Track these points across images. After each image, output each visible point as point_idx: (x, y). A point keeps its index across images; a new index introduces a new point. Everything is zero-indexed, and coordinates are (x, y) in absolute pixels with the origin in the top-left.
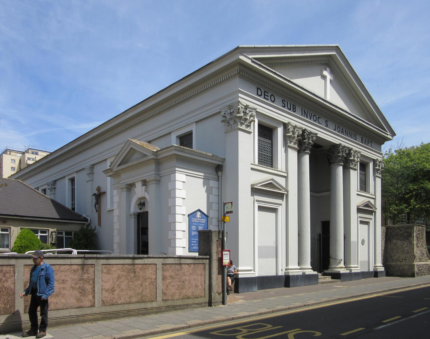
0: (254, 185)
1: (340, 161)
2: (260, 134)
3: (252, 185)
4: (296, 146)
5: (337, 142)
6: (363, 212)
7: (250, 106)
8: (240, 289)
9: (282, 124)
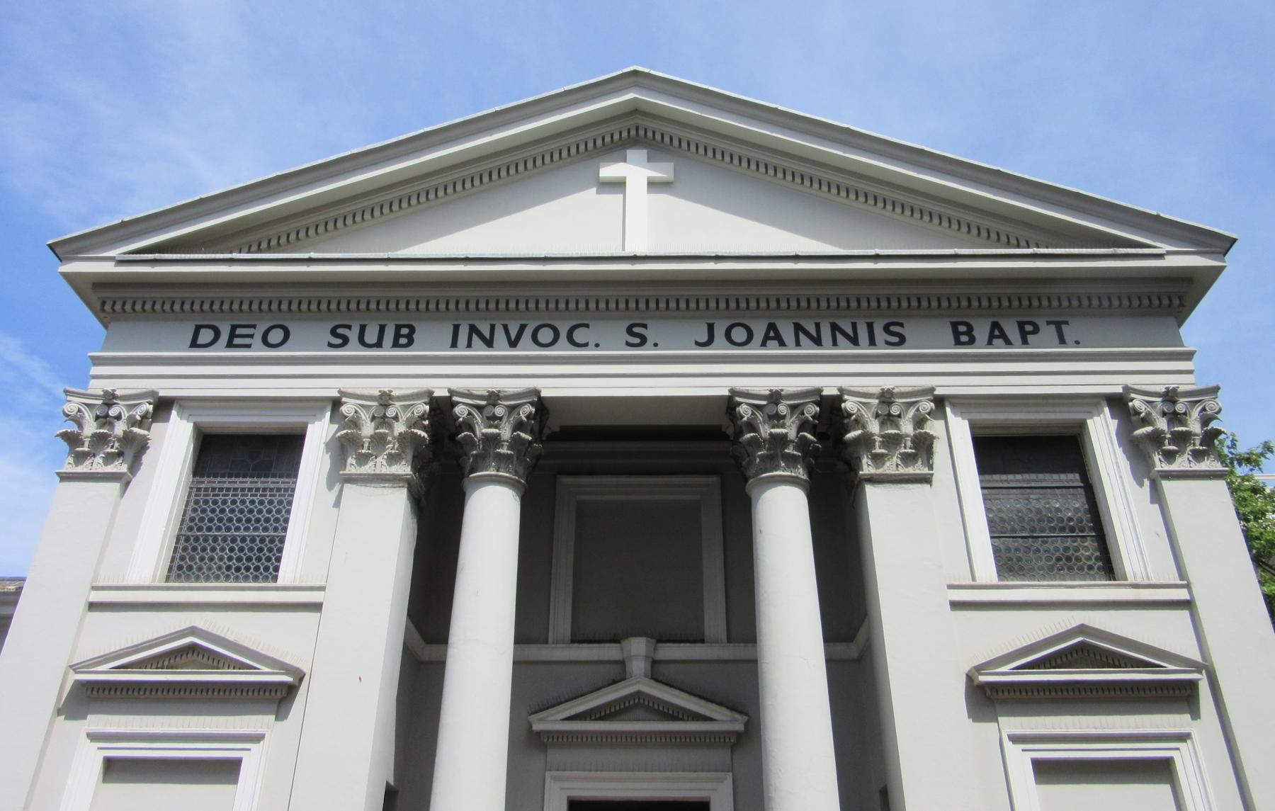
0: (979, 669)
1: (771, 461)
2: (984, 466)
3: (970, 678)
5: (719, 388)
6: (1038, 702)
7: (1182, 389)
9: (1104, 403)
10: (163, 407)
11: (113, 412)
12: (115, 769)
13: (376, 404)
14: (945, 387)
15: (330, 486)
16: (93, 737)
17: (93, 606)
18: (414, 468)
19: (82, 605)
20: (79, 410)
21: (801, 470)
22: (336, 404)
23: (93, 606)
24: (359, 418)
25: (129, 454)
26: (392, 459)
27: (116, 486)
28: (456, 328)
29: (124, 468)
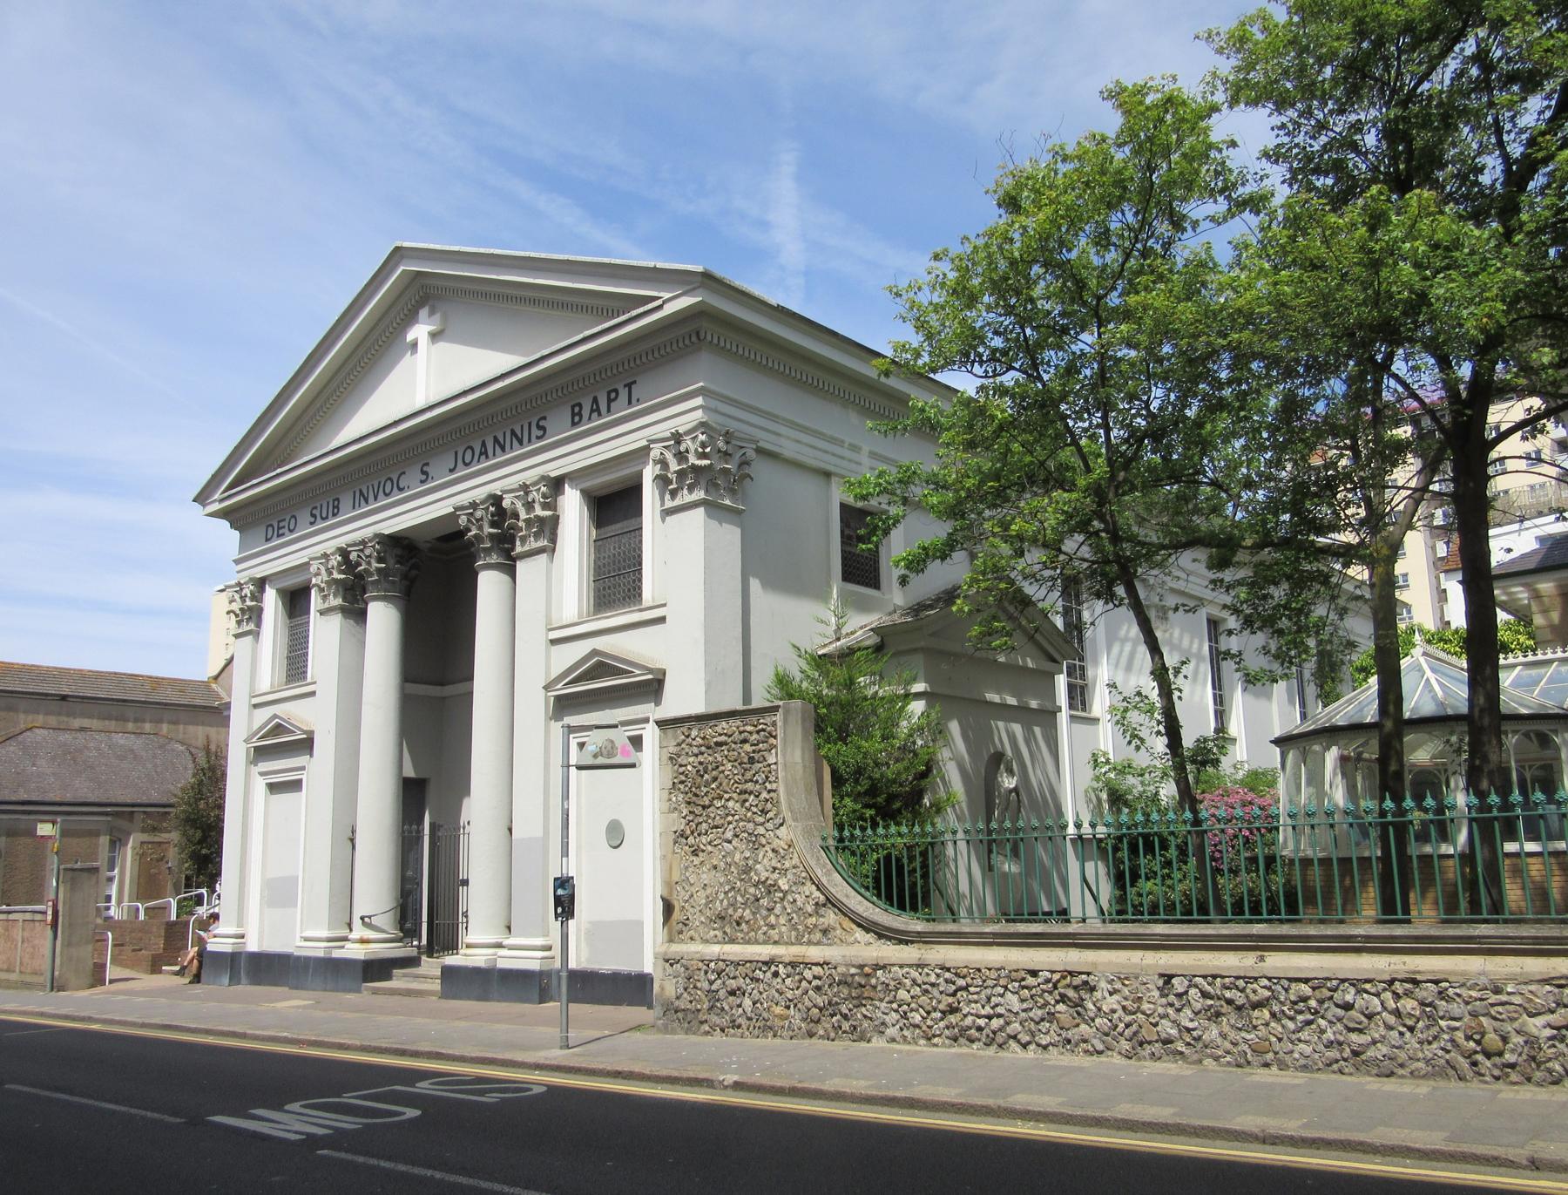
4: (338, 601)
12: (274, 788)
14: (554, 469)
16: (262, 774)
17: (554, 642)
19: (543, 642)
23: (554, 642)
27: (250, 637)
29: (252, 626)
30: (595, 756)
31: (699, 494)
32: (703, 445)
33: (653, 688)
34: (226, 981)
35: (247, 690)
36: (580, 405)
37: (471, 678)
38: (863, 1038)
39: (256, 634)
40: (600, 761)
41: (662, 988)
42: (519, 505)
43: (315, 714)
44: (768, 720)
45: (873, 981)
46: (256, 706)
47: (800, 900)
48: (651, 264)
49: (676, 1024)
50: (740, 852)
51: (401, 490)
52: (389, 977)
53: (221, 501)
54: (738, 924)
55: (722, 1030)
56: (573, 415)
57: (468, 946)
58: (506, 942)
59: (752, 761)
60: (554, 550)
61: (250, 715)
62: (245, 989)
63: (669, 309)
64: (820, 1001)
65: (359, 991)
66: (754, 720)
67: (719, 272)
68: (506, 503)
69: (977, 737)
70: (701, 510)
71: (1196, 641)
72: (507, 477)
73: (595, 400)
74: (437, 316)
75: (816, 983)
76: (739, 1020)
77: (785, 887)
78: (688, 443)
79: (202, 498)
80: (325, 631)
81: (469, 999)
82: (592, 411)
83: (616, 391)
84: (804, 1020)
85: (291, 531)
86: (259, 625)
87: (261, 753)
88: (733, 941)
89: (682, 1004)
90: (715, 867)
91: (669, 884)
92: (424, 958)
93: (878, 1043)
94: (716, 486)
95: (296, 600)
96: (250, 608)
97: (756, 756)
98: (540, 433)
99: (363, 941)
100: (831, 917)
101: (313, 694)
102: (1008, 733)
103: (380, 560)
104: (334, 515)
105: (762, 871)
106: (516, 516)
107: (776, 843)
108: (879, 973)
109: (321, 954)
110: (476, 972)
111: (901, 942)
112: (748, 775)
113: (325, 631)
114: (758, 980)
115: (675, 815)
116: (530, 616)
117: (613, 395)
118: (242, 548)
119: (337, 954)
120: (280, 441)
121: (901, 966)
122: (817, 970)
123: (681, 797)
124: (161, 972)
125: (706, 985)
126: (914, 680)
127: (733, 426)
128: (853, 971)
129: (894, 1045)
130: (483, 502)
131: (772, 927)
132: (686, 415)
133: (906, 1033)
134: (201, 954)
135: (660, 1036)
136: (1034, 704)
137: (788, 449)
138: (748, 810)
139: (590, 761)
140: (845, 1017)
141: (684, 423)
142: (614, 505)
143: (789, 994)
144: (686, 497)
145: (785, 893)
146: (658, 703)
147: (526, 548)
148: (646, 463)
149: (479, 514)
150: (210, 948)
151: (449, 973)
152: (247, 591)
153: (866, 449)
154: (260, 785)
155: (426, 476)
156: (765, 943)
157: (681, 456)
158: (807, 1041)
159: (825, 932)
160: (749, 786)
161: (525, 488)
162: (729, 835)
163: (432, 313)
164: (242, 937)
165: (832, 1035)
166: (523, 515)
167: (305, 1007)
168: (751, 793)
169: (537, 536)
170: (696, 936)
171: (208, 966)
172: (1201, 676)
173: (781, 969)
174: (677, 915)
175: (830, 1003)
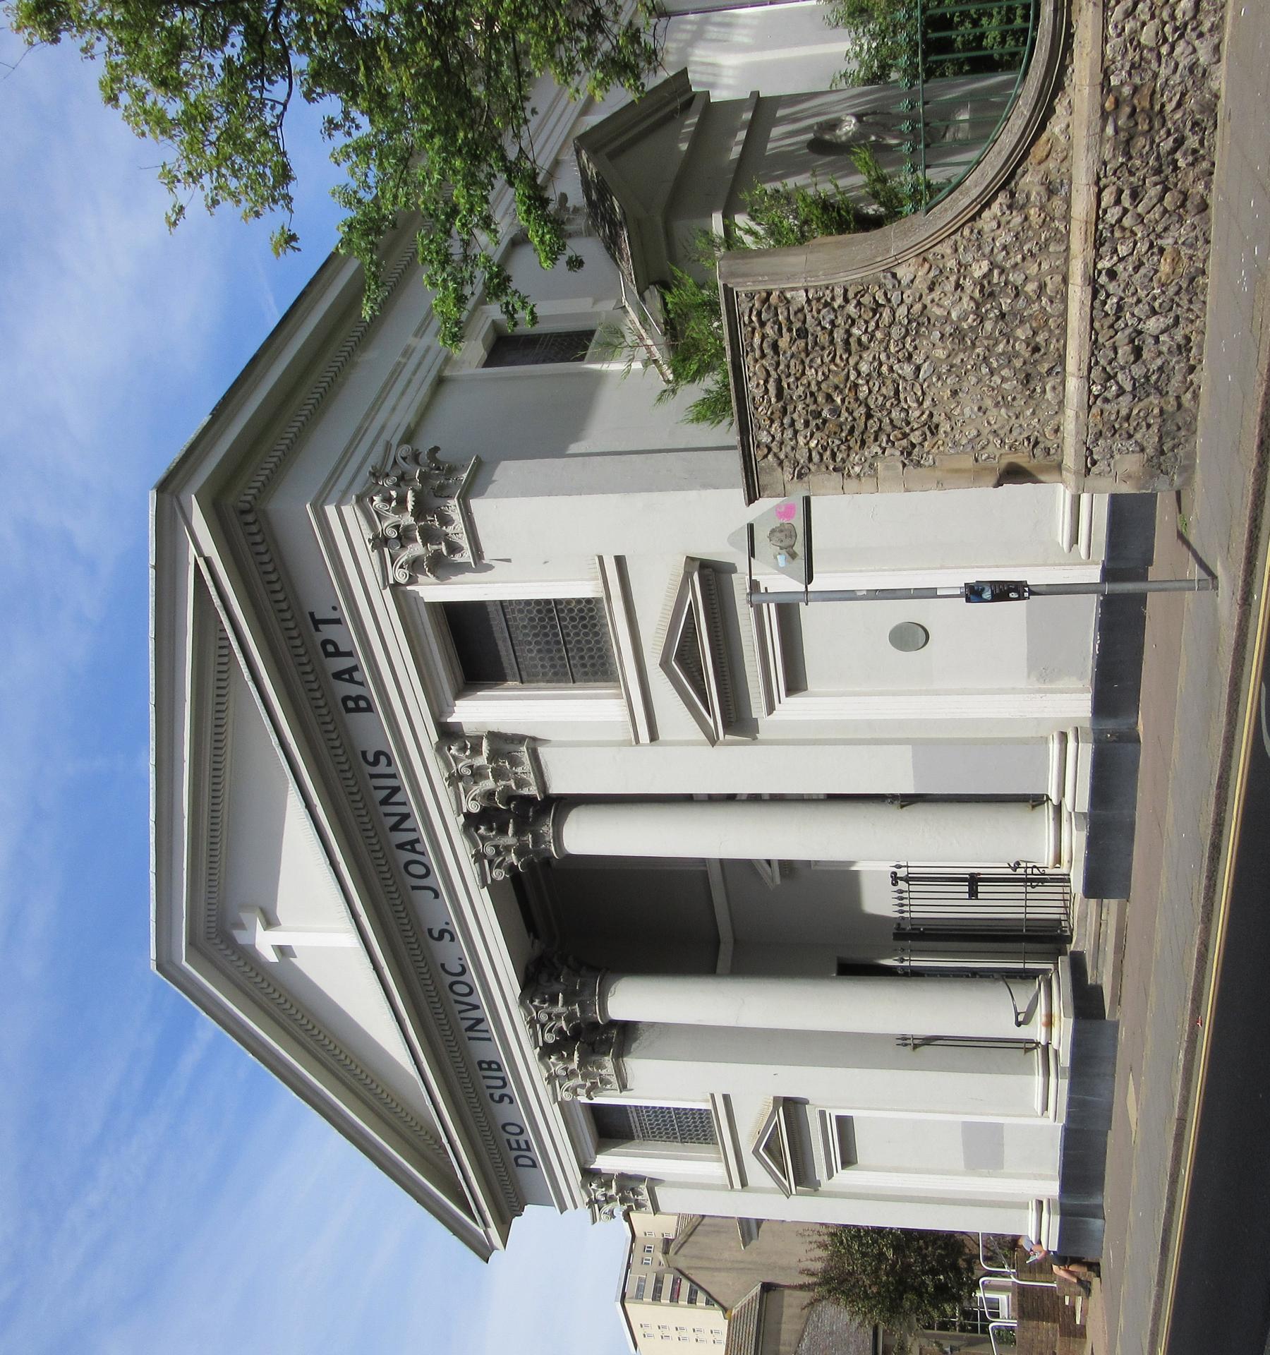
4: (608, 1061)
5: (483, 900)
8: (1090, 1258)
10: (448, 734)
11: (393, 534)
12: (848, 1160)
13: (386, 550)
14: (429, 736)
15: (489, 567)
16: (830, 1175)
17: (654, 737)
18: (606, 1053)
19: (656, 749)
20: (401, 567)
21: (545, 828)
22: (395, 587)
23: (654, 737)
24: (407, 562)
25: (632, 1184)
26: (601, 1066)
27: (542, 751)
28: (470, 1039)
29: (643, 1188)
30: (793, 556)
31: (453, 508)
32: (388, 500)
33: (711, 576)
34: (1098, 1223)
35: (724, 1194)
36: (346, 699)
37: (703, 861)
38: (1210, 108)
39: (653, 1183)
40: (799, 548)
41: (1128, 477)
42: (477, 790)
43: (752, 1091)
44: (743, 306)
45: (1126, 90)
46: (744, 1183)
47: (1005, 237)
48: (152, 572)
49: (1180, 452)
50: (934, 348)
51: (464, 970)
52: (1098, 990)
53: (486, 1224)
54: (1036, 349)
55: (1192, 369)
56: (358, 709)
57: (1058, 859)
58: (1055, 802)
59: (803, 333)
60: (534, 739)
61: (667, 744)
62: (1109, 1198)
63: (210, 549)
64: (1153, 192)
65: (1116, 1025)
66: (743, 332)
67: (160, 473)
68: (474, 808)
69: (789, 163)
70: (475, 504)
71: (683, 27)
72: (440, 807)
73: (401, 846)
74: (245, 917)
75: (1126, 197)
76: (1179, 338)
77: (985, 265)
78: (463, 768)
79: (484, 1251)
80: (650, 1082)
81: (1130, 854)
82: (352, 680)
83: (325, 643)
84: (1181, 220)
85: (522, 1131)
86: (641, 1179)
87: (804, 1177)
88: (1062, 359)
89: (1151, 441)
90: (955, 393)
91: (976, 476)
92: (1071, 947)
93: (1220, 81)
94: (442, 487)
95: (611, 1127)
96: (620, 1190)
97: (797, 325)
98: (383, 759)
99: (1049, 1023)
100: (1030, 182)
101: (726, 1098)
102: (780, 138)
103: (554, 1001)
104: (499, 1069)
105: (959, 308)
106: (490, 795)
107: (921, 285)
108: (1114, 81)
109: (1065, 1084)
110: (1093, 843)
111: (1068, 47)
112: (823, 339)
113: (650, 1082)
114: (1120, 308)
115: (879, 465)
116: (618, 762)
117: (330, 648)
118: (545, 1202)
119: (1065, 1060)
120: (415, 1149)
121: (1105, 40)
122: (1107, 198)
123: (855, 458)
124: (1083, 1327)
125: (1125, 401)
126: (707, 233)
127: (368, 468)
128: (1110, 130)
129: (1224, 48)
130: (475, 845)
131: (1042, 287)
132: (349, 527)
133: (1206, 27)
134: (1063, 1258)
135: (1198, 477)
136: (747, 116)
137: (404, 417)
138: (872, 337)
139: (801, 563)
140: (1179, 142)
141: (361, 533)
142: (474, 647)
143: (1142, 247)
144: (457, 531)
145: (993, 266)
146: (731, 569)
147: (531, 778)
148: (416, 597)
149: (490, 851)
150: (1054, 1247)
151: (1096, 886)
152: (599, 1194)
153: (411, 340)
154: (845, 1178)
155: (445, 933)
156: (1065, 300)
157: (404, 537)
158: (1213, 211)
159: (1051, 191)
160: (839, 335)
161: (454, 779)
162: (908, 370)
163: (241, 926)
164: (1040, 1203)
165: (1205, 165)
166: (489, 784)
167: (1137, 1093)
168: (848, 333)
169: (515, 762)
170: (1053, 423)
171: (1076, 1251)
172: (727, 20)
173: (1105, 264)
174: (1022, 459)
175: (1158, 171)
